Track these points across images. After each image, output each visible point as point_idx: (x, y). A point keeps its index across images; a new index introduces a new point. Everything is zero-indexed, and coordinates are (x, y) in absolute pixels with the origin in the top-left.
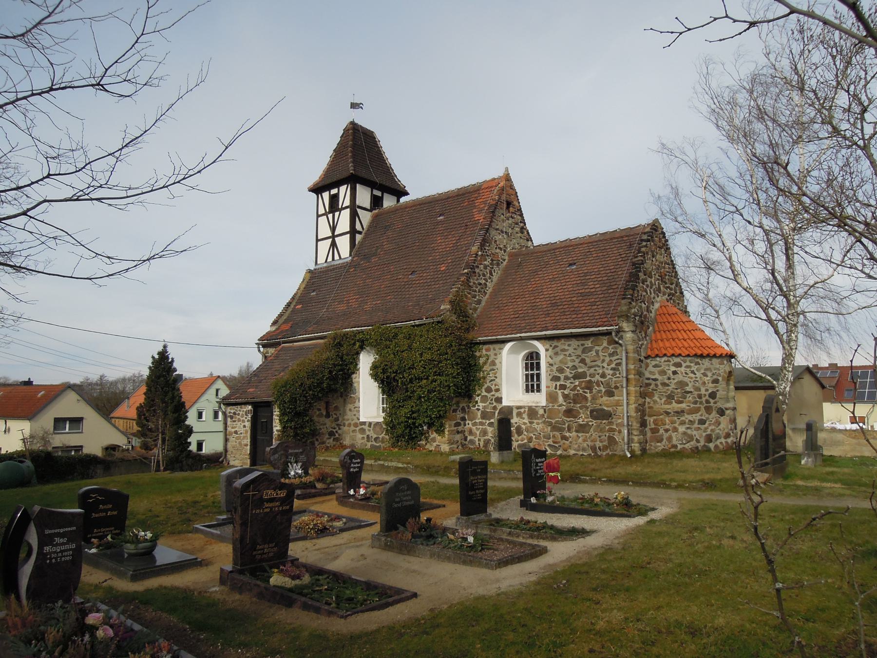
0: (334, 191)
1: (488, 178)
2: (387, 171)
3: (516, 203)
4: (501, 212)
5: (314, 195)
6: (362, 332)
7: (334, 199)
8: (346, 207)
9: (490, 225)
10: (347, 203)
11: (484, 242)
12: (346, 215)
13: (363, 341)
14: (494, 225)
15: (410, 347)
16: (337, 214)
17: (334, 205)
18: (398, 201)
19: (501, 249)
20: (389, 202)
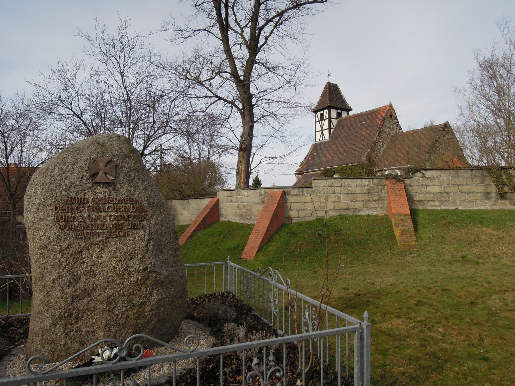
0: (322, 112)
1: (383, 106)
2: (343, 101)
5: (313, 114)
6: (334, 168)
7: (322, 115)
8: (327, 119)
10: (327, 117)
11: (380, 133)
12: (327, 121)
13: (335, 171)
14: (384, 125)
16: (323, 121)
17: (322, 118)
18: (348, 114)
20: (344, 115)
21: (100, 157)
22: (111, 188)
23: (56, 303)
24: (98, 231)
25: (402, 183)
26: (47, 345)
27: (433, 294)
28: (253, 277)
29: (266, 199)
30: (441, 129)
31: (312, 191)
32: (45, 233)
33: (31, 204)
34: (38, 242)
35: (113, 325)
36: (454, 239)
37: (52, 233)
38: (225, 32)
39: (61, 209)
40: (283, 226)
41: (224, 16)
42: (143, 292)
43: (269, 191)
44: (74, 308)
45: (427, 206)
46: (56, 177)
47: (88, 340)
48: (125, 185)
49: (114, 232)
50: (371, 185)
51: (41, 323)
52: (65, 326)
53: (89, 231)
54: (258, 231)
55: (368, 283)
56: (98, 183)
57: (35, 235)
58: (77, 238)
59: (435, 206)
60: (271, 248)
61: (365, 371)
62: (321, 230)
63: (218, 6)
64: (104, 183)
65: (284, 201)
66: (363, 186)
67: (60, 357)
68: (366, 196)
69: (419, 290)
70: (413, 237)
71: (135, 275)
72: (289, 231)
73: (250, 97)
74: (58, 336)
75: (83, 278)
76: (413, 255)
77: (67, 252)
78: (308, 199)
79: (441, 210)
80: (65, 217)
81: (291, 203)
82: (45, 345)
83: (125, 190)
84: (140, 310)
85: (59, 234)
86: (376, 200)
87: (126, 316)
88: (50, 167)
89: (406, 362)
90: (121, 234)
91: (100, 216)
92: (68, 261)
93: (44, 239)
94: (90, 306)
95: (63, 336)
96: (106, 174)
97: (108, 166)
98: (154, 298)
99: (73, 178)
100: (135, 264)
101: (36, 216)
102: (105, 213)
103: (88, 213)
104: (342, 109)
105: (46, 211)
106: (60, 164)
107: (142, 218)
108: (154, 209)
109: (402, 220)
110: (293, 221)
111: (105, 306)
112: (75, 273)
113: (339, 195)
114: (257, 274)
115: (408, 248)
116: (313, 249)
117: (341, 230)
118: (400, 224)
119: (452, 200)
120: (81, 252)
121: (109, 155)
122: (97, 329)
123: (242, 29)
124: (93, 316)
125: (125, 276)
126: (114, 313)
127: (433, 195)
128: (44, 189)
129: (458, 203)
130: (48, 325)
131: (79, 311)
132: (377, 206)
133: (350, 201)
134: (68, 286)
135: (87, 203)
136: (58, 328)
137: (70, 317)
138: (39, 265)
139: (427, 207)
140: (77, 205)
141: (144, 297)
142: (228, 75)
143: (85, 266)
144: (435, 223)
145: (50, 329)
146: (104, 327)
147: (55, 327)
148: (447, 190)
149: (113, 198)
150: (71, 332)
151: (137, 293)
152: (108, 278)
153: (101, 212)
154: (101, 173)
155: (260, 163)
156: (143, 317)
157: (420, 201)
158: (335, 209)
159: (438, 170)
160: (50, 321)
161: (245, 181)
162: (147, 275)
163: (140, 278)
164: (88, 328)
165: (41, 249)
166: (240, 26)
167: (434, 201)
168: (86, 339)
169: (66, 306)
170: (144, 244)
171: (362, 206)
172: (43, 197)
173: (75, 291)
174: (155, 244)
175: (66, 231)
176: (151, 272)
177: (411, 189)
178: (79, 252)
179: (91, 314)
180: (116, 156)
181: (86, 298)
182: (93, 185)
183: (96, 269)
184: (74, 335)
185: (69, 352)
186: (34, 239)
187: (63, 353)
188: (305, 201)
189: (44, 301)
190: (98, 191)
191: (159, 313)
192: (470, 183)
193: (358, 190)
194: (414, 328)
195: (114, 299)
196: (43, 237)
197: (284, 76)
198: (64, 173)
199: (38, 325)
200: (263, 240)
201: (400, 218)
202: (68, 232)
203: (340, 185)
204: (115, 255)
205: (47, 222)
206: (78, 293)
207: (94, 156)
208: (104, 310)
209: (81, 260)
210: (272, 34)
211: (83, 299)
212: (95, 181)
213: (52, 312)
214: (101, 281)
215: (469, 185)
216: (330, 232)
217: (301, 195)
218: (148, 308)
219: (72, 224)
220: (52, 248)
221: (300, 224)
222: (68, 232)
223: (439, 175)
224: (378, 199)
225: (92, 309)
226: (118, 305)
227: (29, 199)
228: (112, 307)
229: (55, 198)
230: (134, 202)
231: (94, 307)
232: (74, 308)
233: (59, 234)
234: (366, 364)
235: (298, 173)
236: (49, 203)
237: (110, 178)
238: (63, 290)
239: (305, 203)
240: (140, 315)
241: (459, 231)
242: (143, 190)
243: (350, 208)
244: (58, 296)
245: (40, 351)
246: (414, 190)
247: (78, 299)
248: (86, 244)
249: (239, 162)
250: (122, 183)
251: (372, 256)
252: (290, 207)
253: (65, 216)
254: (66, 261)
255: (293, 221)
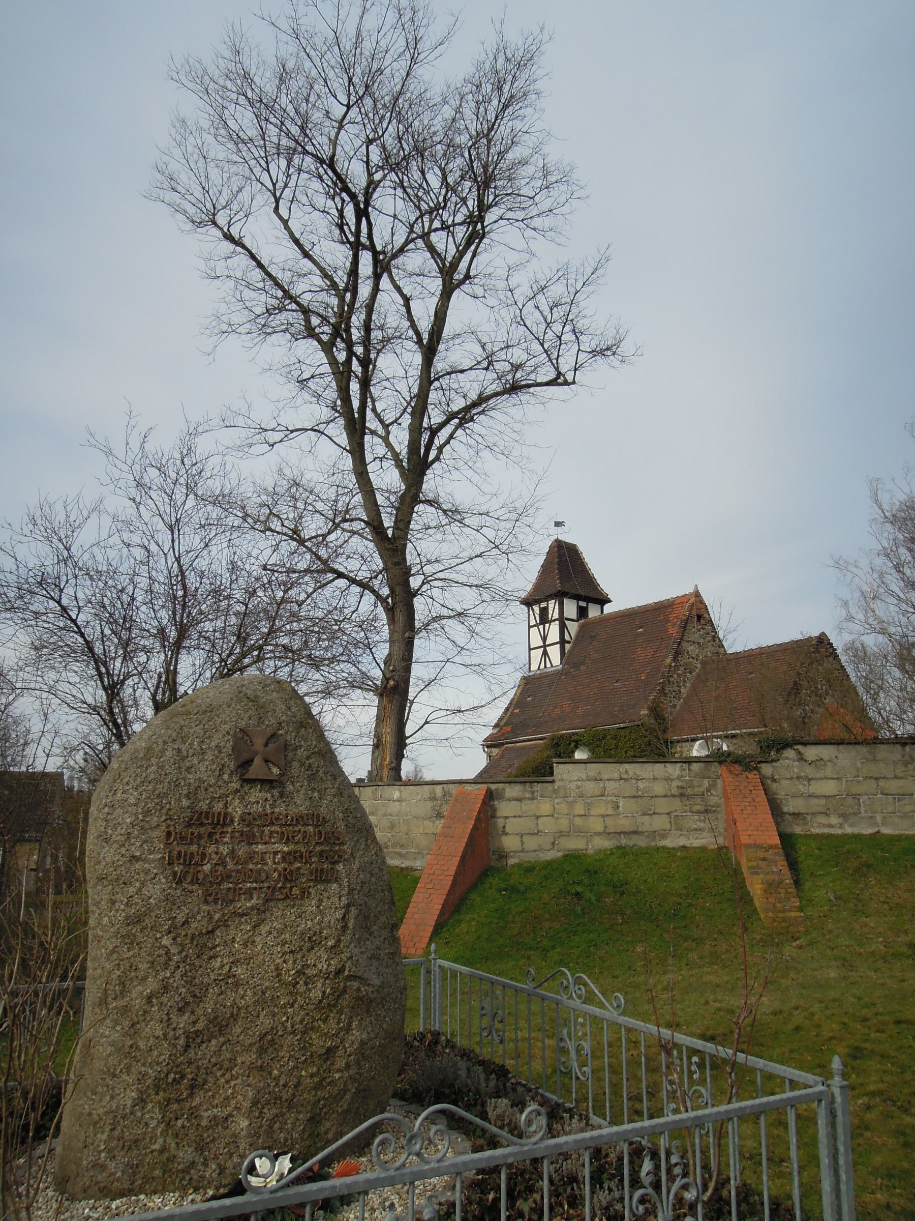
0: (543, 605)
2: (590, 581)
3: (706, 615)
4: (693, 627)
6: (576, 734)
7: (544, 612)
8: (555, 620)
9: (682, 639)
10: (556, 616)
11: (677, 654)
14: (685, 638)
15: (617, 747)
16: (547, 626)
17: (544, 618)
19: (693, 658)
20: (594, 612)
21: (254, 726)
22: (276, 793)
23: (151, 1050)
24: (248, 885)
25: (755, 772)
26: (122, 1153)
27: (878, 1031)
28: (510, 992)
29: (445, 810)
30: (812, 650)
31: (555, 791)
32: (140, 889)
33: (111, 824)
34: (124, 910)
35: (268, 1103)
36: (884, 902)
37: (156, 890)
38: (358, 435)
39: (178, 836)
40: (486, 872)
41: (356, 404)
42: (332, 1026)
43: (453, 789)
44: (190, 1063)
45: (812, 826)
46: (167, 767)
47: (214, 1140)
48: (302, 786)
49: (281, 888)
50: (687, 778)
51: (112, 1097)
52: (167, 1106)
53: (231, 885)
54: (431, 886)
55: (719, 1010)
56: (252, 781)
57: (117, 893)
58: (206, 902)
59: (831, 826)
60: (464, 927)
61: (843, 1187)
62: (579, 883)
63: (344, 384)
64: (263, 782)
65: (489, 814)
66: (668, 779)
67: (146, 1182)
68: (677, 802)
69: (844, 1024)
70: (792, 900)
71: (320, 985)
72: (503, 886)
73: (407, 573)
74: (150, 1130)
75: (213, 991)
76: (798, 942)
77: (184, 933)
78: (545, 807)
79: (844, 835)
80: (185, 855)
81: (506, 817)
82: (116, 1152)
83: (302, 796)
84: (325, 1067)
85: (172, 892)
86: (698, 812)
87: (295, 1080)
88: (155, 746)
89: (885, 1182)
90: (296, 891)
91: (254, 852)
92: (184, 954)
93: (137, 904)
94: (222, 1057)
95: (160, 1130)
96: (266, 761)
97: (271, 746)
98: (353, 1038)
99: (203, 770)
100: (321, 961)
101: (123, 850)
102: (264, 846)
103: (230, 846)
104: (589, 600)
105: (147, 841)
106: (174, 740)
107: (336, 858)
108: (355, 839)
109: (764, 859)
110: (512, 861)
111: (254, 1056)
112: (197, 980)
113: (614, 799)
114: (525, 987)
115: (784, 924)
116: (565, 930)
117: (626, 884)
118: (761, 868)
119: (866, 812)
120: (213, 931)
121: (271, 721)
122: (235, 1113)
123: (386, 427)
124: (227, 1082)
125: (298, 986)
126: (270, 1073)
127: (823, 802)
128: (144, 793)
129: (879, 818)
130: (129, 1103)
131: (198, 1068)
132: (702, 825)
133: (640, 813)
134: (180, 1010)
135: (229, 825)
136: (149, 1112)
137: (179, 1083)
138: (117, 962)
139: (812, 830)
140: (210, 829)
141: (333, 1035)
142: (360, 525)
143: (217, 963)
144: (837, 866)
145: (131, 1113)
146: (251, 1107)
147: (143, 1108)
148: (855, 790)
149: (280, 814)
150: (177, 1119)
151: (319, 1027)
152: (264, 993)
153: (257, 843)
154: (258, 761)
155: (426, 722)
156: (329, 1084)
157: (796, 815)
158: (606, 833)
159: (831, 744)
160: (132, 1094)
161: (393, 765)
162: (342, 984)
163: (328, 991)
164: (215, 1110)
165: (128, 925)
166: (381, 421)
167: (827, 815)
168: (209, 1137)
169: (173, 1058)
170: (339, 915)
171: (668, 827)
172: (140, 811)
173: (195, 1023)
174: (358, 915)
175: (186, 886)
176: (351, 977)
177: (774, 786)
178: (208, 932)
179: (223, 1075)
180: (284, 725)
181: (215, 1037)
182: (242, 786)
183: (239, 970)
184: (183, 1127)
185: (171, 1170)
186: (113, 902)
187: (157, 1172)
188: (538, 814)
189: (123, 1046)
190: (253, 799)
191: (360, 1074)
192: (901, 774)
193: (659, 788)
194: (868, 1108)
195: (273, 1040)
196: (137, 899)
197: (484, 530)
198: (184, 759)
199: (104, 1103)
200: (444, 905)
201: (761, 854)
202: (190, 887)
203: (616, 776)
204: (280, 939)
205: (146, 865)
206: (200, 1026)
207: (242, 724)
208: (252, 1067)
209: (211, 950)
210: (452, 441)
211: (210, 1041)
212: (246, 776)
213: (140, 1073)
214: (249, 998)
215: (901, 778)
216: (603, 888)
217: (528, 799)
218: (341, 1063)
219: (199, 868)
220: (153, 924)
221: (529, 869)
222: (190, 887)
223: (833, 756)
224: (703, 809)
225: (226, 1064)
226: (281, 1054)
227: (108, 814)
228: (267, 1059)
229: (167, 814)
230: (318, 820)
231: (231, 1060)
232: (190, 1063)
233: (172, 892)
234: (846, 1173)
235: (490, 743)
236: (154, 825)
237: (276, 771)
238: (169, 1019)
239: (538, 817)
240: (324, 1079)
241: (891, 883)
242: (334, 796)
243: (640, 829)
244: (156, 1034)
245: (103, 1167)
246: (782, 789)
247: (199, 1040)
248: (223, 915)
249: (380, 720)
250: (297, 782)
251: (708, 946)
252: (504, 827)
253: (185, 852)
254: (180, 952)
255: (512, 861)
